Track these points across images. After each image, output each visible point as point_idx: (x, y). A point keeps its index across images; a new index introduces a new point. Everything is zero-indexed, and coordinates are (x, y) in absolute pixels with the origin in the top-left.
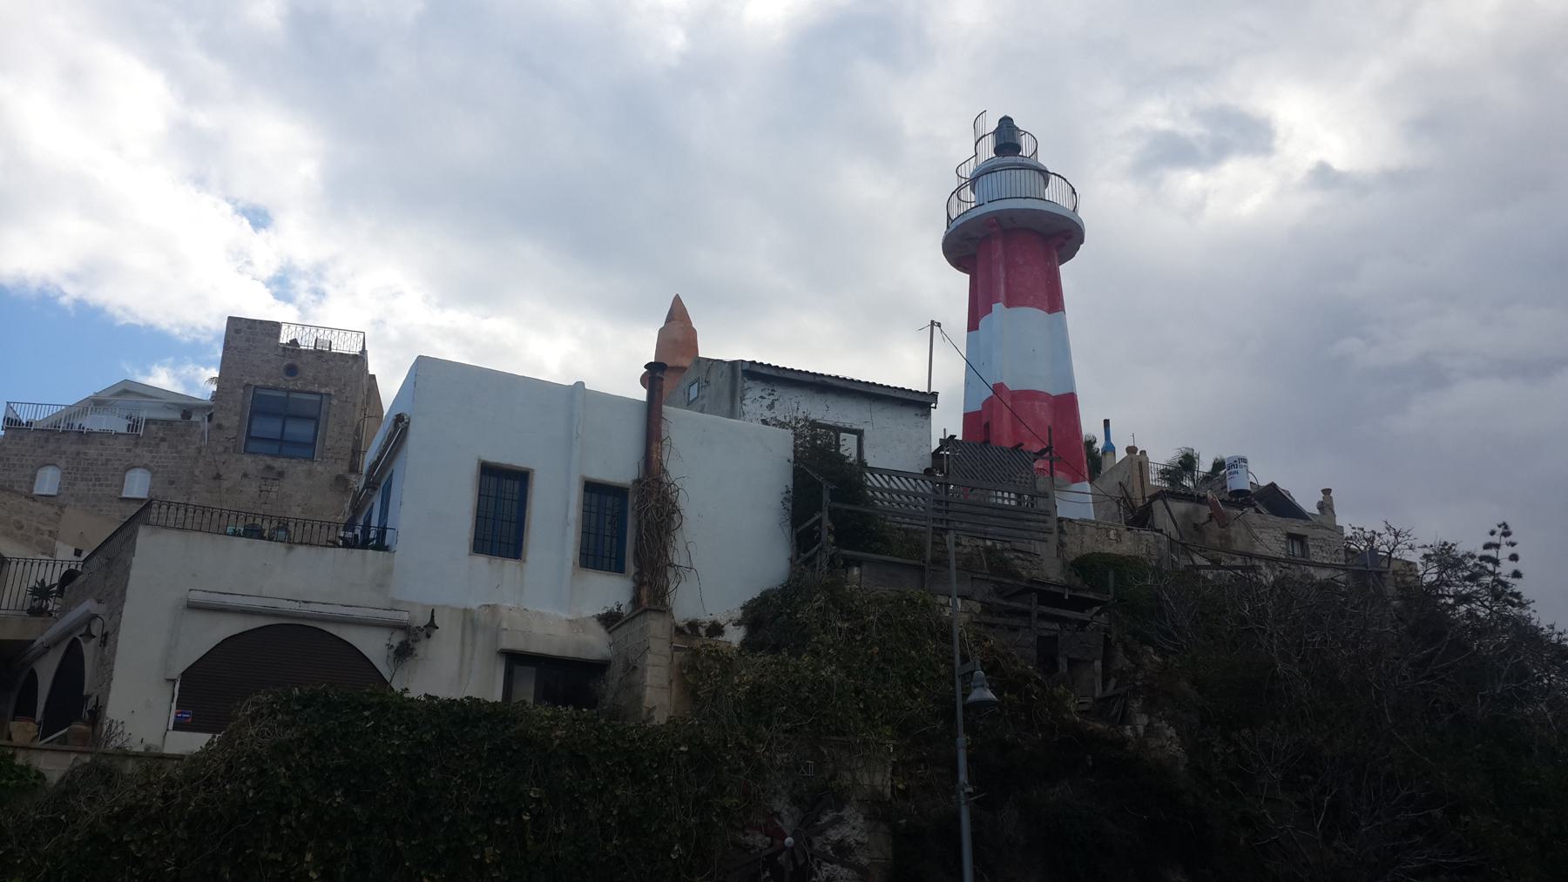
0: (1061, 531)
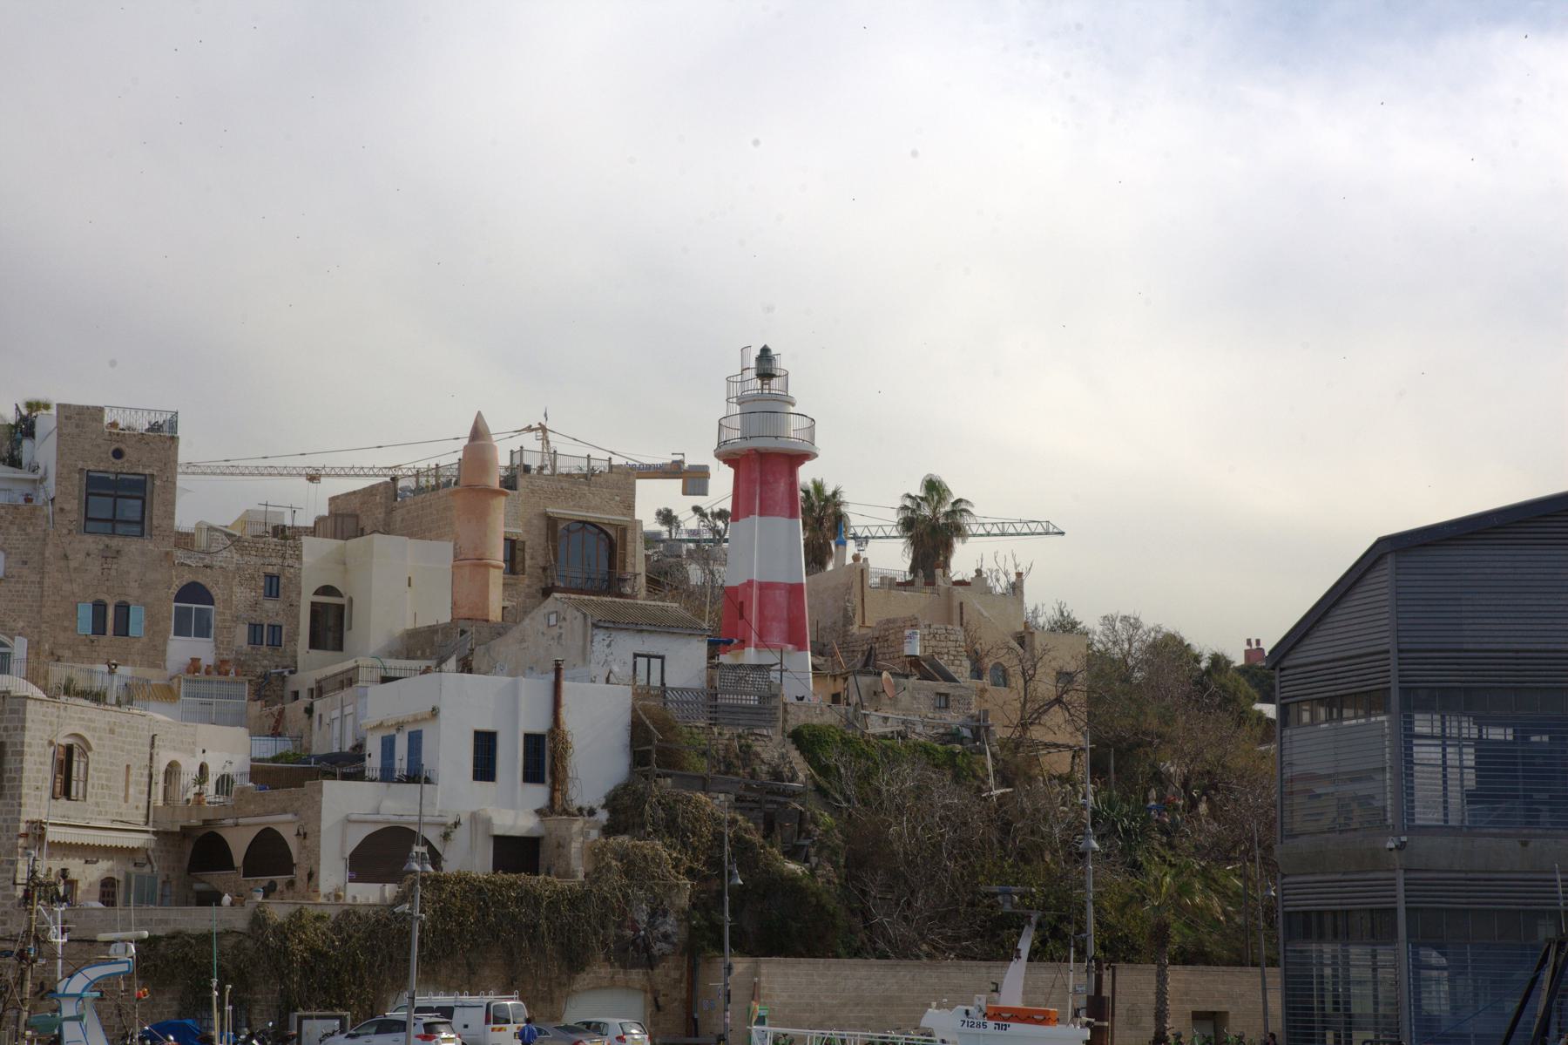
0: (785, 711)
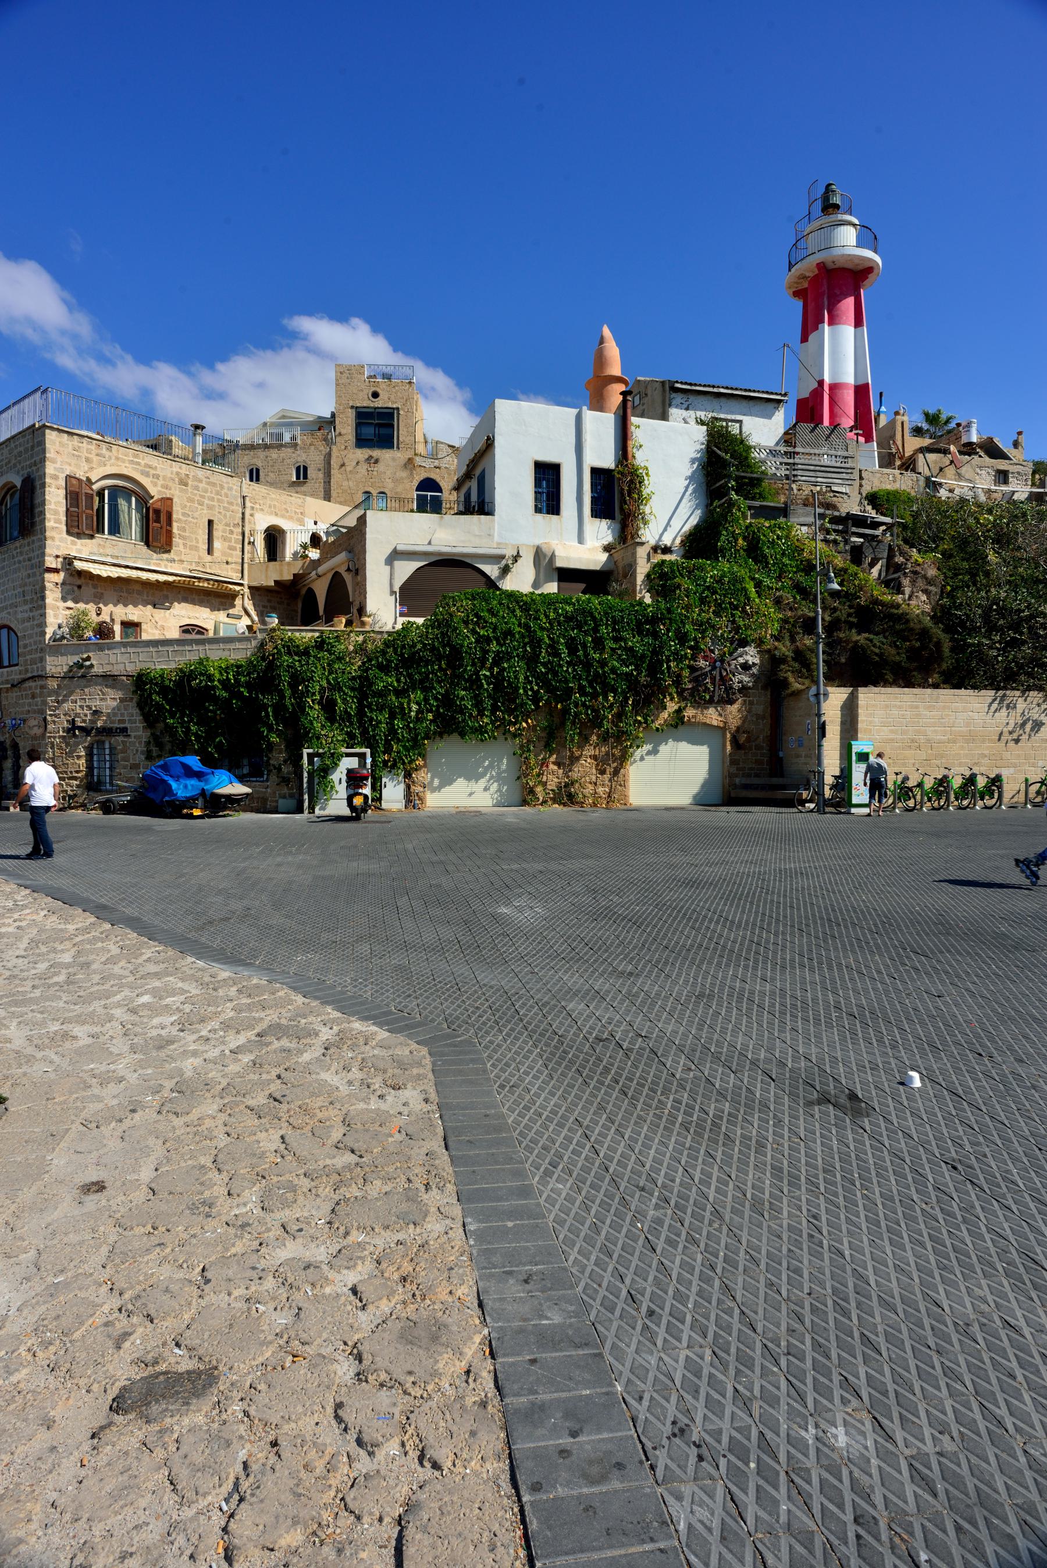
0: (861, 478)
